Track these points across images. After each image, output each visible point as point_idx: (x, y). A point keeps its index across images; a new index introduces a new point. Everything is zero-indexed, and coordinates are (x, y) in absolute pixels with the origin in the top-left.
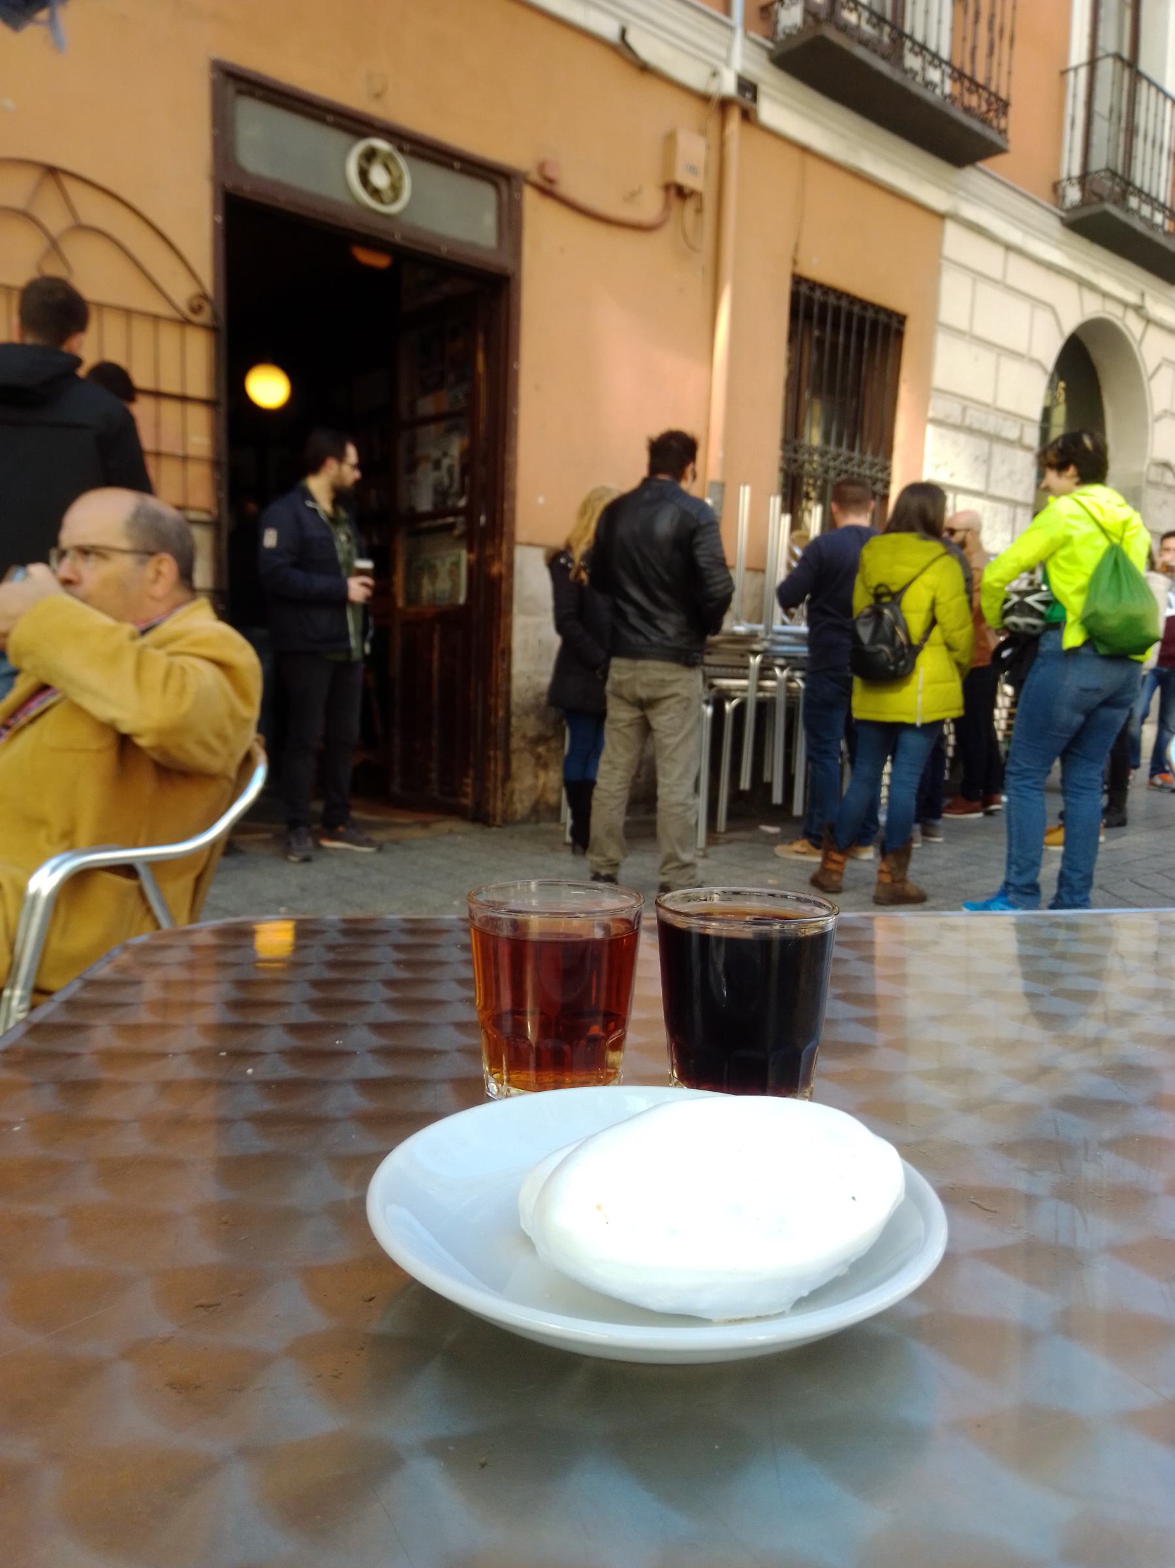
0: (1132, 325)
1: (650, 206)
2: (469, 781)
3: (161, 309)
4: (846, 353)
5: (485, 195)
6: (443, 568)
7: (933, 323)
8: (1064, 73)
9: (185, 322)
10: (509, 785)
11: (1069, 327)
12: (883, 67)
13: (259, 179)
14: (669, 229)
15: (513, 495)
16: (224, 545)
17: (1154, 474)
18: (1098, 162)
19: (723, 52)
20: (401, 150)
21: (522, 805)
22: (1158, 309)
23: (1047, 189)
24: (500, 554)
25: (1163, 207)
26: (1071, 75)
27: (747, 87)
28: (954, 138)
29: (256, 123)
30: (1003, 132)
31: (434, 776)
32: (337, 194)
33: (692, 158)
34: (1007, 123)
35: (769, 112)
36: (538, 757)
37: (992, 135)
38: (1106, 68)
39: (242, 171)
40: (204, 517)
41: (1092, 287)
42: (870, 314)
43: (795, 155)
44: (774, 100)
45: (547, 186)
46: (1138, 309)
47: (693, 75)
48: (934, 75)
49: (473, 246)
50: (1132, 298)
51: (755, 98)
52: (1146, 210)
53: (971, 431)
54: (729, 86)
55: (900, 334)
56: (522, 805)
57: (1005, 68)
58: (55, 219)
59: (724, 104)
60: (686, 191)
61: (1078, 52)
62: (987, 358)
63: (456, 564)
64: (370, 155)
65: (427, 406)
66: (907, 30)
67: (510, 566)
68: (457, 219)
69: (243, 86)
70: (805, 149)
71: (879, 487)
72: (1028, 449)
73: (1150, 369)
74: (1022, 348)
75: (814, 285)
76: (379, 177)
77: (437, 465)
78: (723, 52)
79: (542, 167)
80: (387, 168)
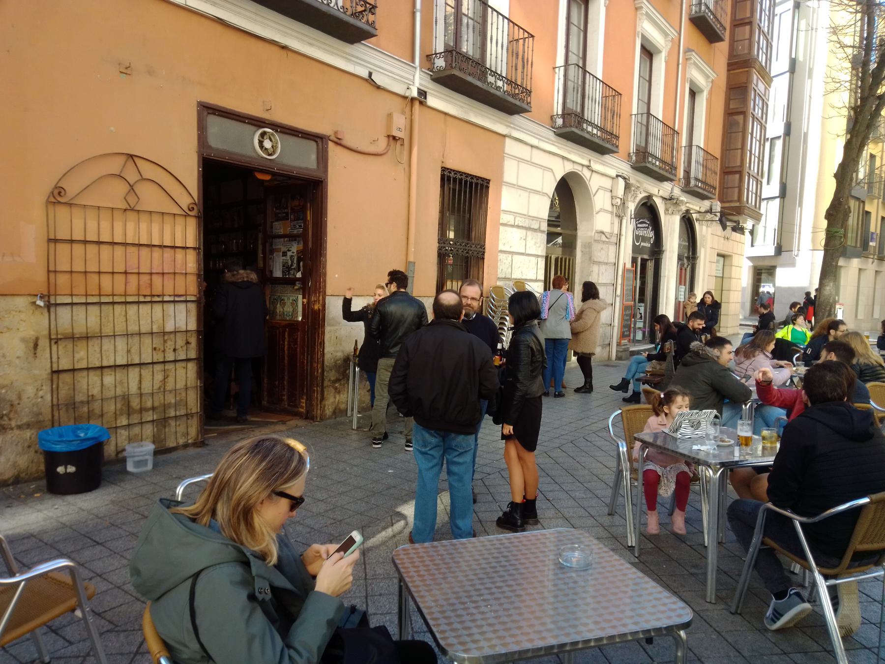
0: (586, 174)
1: (382, 144)
2: (304, 401)
3: (177, 211)
4: (465, 197)
5: (312, 145)
6: (288, 302)
7: (501, 183)
8: (554, 68)
9: (186, 215)
10: (323, 403)
11: (559, 178)
12: (479, 84)
13: (217, 150)
14: (389, 153)
15: (325, 274)
16: (202, 309)
17: (597, 237)
18: (570, 104)
19: (412, 78)
20: (276, 131)
21: (329, 411)
22: (595, 166)
23: (548, 120)
25: (597, 127)
26: (557, 70)
27: (423, 93)
28: (509, 105)
29: (215, 124)
30: (529, 103)
31: (285, 398)
32: (250, 153)
33: (400, 122)
35: (431, 101)
36: (336, 388)
37: (524, 106)
38: (572, 70)
39: (210, 147)
40: (193, 298)
41: (568, 160)
42: (474, 181)
43: (442, 116)
44: (435, 96)
45: (339, 141)
46: (588, 167)
47: (399, 89)
48: (500, 84)
49: (307, 169)
50: (586, 163)
51: (425, 98)
52: (590, 129)
53: (518, 227)
54: (415, 94)
55: (488, 187)
56: (329, 411)
57: (530, 49)
58: (132, 177)
59: (413, 99)
61: (560, 61)
62: (525, 195)
63: (296, 301)
64: (263, 135)
65: (280, 228)
66: (488, 66)
68: (299, 158)
69: (210, 111)
70: (446, 114)
71: (480, 255)
72: (543, 232)
73: (594, 192)
74: (539, 189)
75: (450, 171)
76: (267, 144)
77: (285, 254)
78: (412, 78)
79: (336, 133)
80: (271, 140)
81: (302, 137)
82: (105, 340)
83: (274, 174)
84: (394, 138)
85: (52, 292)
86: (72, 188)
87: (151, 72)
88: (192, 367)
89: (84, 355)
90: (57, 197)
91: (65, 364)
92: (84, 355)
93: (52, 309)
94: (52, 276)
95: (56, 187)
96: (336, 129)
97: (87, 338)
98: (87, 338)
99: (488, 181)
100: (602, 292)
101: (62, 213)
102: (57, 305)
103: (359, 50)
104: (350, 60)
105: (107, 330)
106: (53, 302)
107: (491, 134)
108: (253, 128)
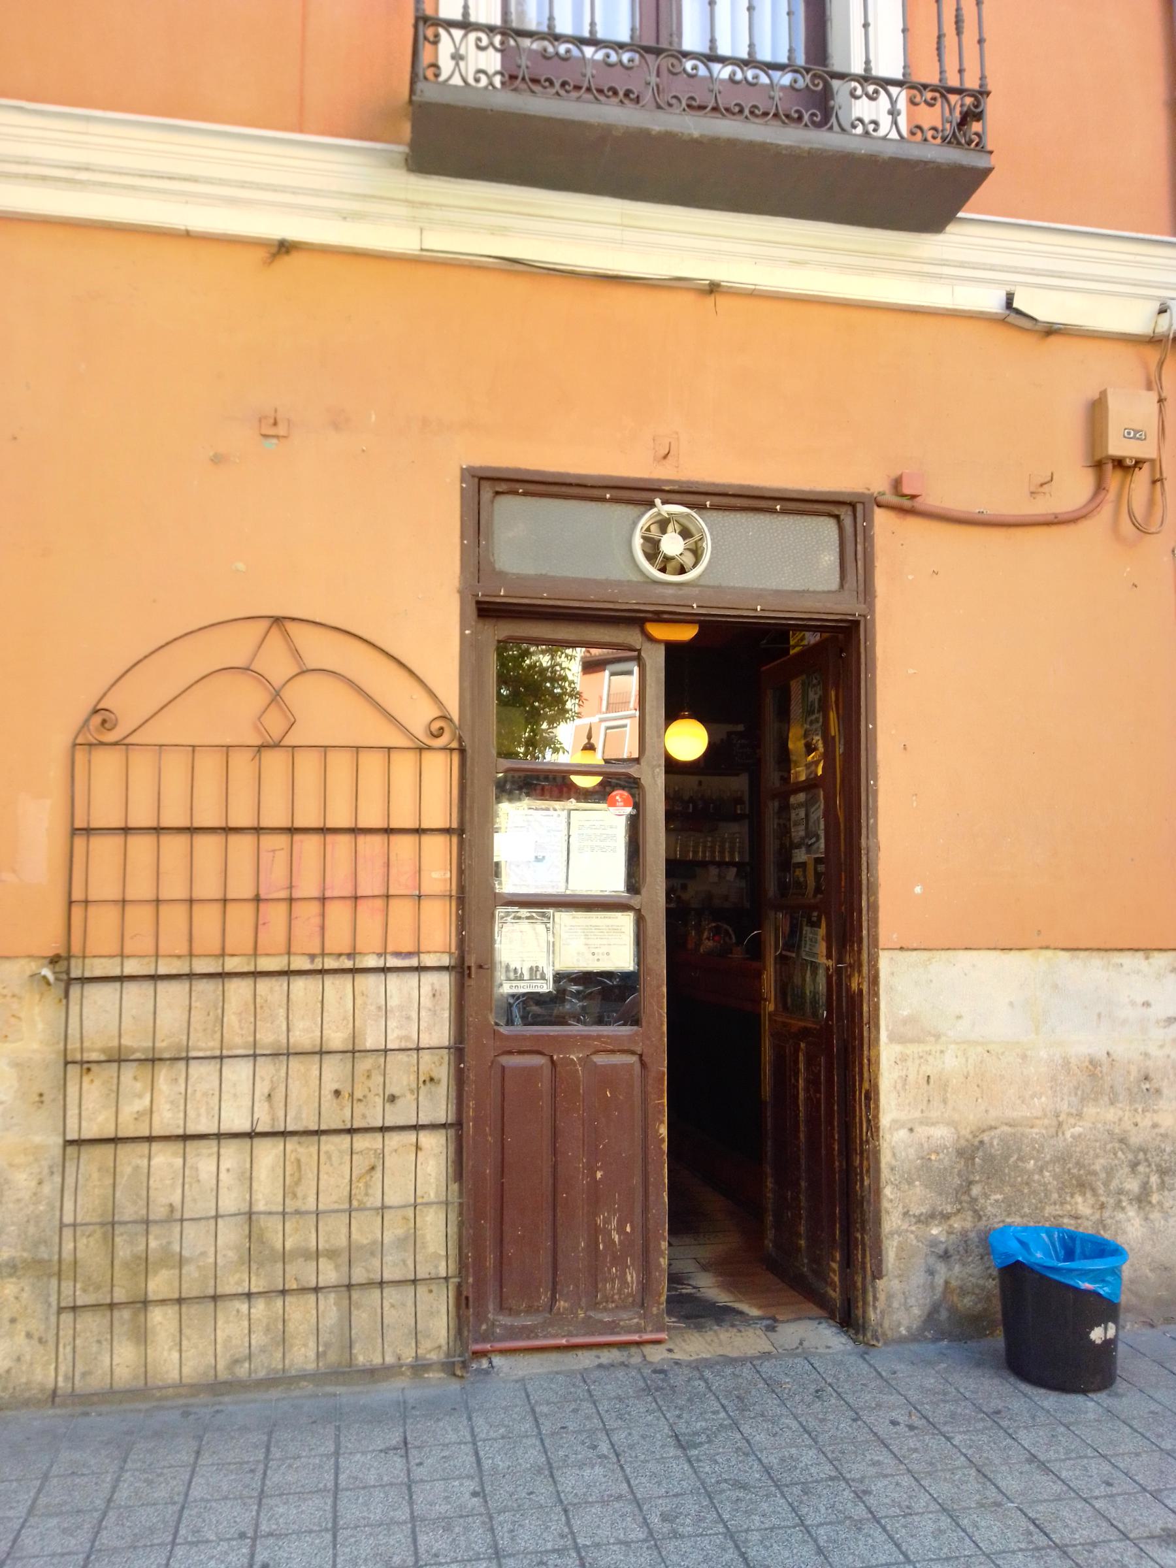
1: (1074, 487)
2: (835, 1266)
3: (399, 740)
5: (827, 529)
15: (873, 889)
20: (699, 507)
24: (860, 965)
31: (802, 1229)
34: (1131, 458)
40: (445, 961)
45: (907, 503)
60: (1128, 462)
67: (875, 980)
69: (503, 487)
76: (672, 545)
79: (897, 484)
81: (784, 512)
82: (196, 1069)
84: (1119, 463)
85: (76, 949)
86: (129, 707)
87: (338, 422)
88: (435, 1145)
89: (164, 1102)
90: (99, 731)
91: (97, 1124)
92: (164, 1102)
93: (75, 991)
94: (77, 911)
95: (96, 711)
96: (895, 474)
97: (153, 1060)
98: (153, 1060)
99: (462, 469)
100: (23, 1334)
101: (107, 764)
102: (84, 980)
103: (959, 241)
105: (204, 1044)
106: (75, 973)
108: (629, 511)
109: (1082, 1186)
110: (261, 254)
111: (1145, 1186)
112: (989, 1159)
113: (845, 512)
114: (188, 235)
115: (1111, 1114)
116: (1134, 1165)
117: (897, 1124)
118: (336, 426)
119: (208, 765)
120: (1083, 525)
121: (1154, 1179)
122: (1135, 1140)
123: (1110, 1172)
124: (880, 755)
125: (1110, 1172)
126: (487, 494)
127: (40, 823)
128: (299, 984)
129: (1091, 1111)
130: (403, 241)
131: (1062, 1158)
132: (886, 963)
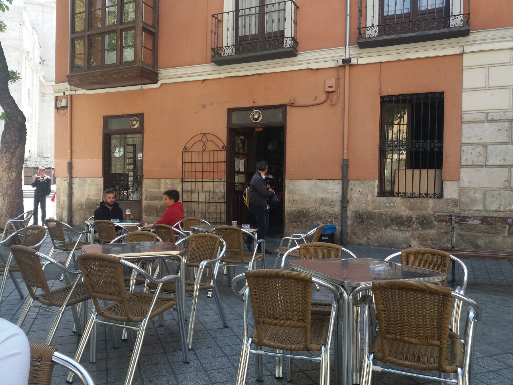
47: (332, 64)
68: (276, 118)
83: (263, 128)
86: (188, 146)
90: (185, 150)
97: (192, 192)
98: (192, 192)
101: (186, 154)
104: (473, 44)
107: (494, 52)
109: (320, 219)
110: (201, 82)
111: (332, 220)
112: (303, 213)
113: (283, 107)
114: (267, 73)
115: (326, 208)
116: (330, 217)
117: (288, 207)
118: (211, 105)
119: (197, 154)
120: (325, 104)
121: (333, 219)
122: (330, 212)
123: (325, 217)
124: (287, 148)
125: (325, 217)
126: (231, 112)
127: (180, 161)
128: (204, 183)
129: (322, 207)
130: (217, 76)
131: (316, 214)
132: (286, 181)
